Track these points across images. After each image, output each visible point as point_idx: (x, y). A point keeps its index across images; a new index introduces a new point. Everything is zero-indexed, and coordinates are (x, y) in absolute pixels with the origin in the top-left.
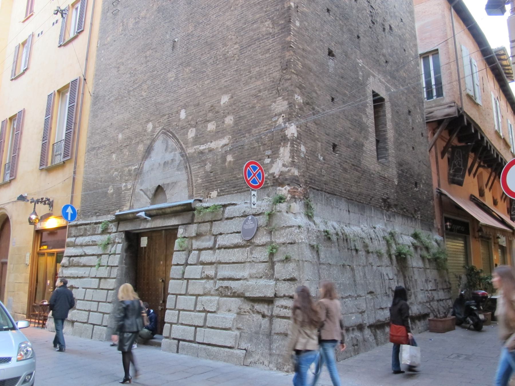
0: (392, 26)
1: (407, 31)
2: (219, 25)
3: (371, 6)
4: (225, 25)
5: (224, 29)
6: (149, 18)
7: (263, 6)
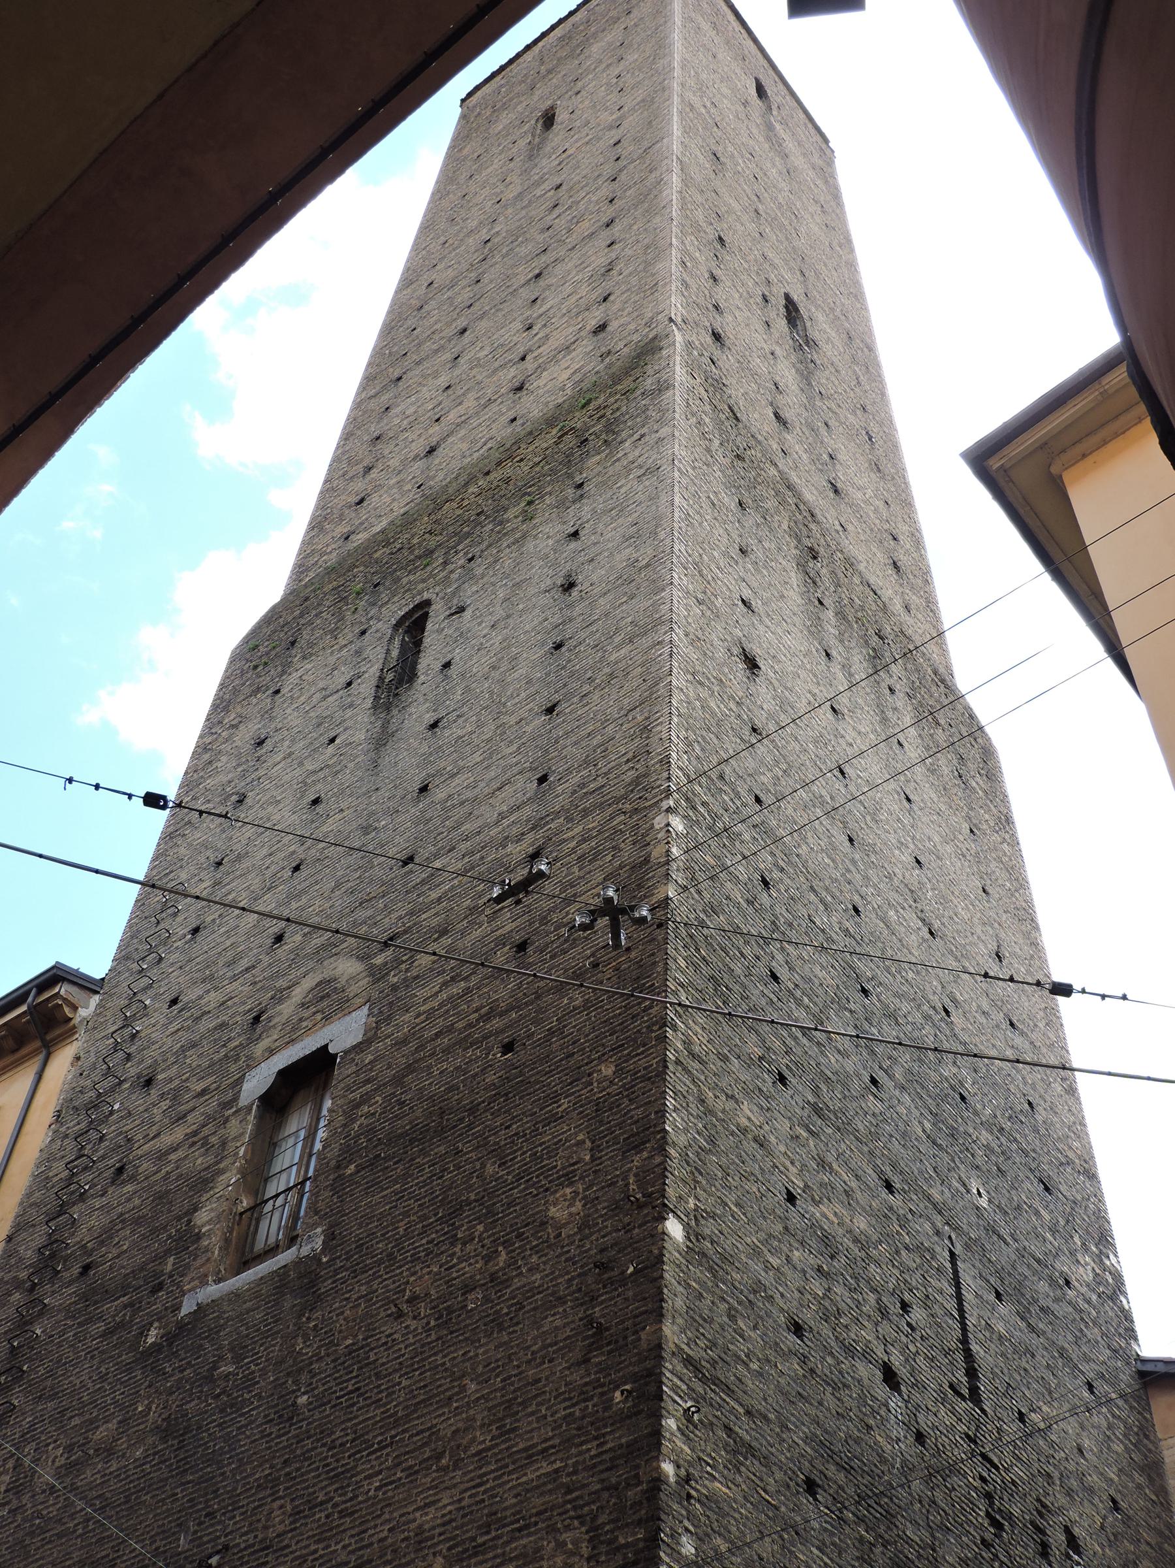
0: (1076, 1531)
1: (1144, 1547)
2: (389, 1521)
3: (984, 1456)
4: (413, 1526)
6: (123, 1456)
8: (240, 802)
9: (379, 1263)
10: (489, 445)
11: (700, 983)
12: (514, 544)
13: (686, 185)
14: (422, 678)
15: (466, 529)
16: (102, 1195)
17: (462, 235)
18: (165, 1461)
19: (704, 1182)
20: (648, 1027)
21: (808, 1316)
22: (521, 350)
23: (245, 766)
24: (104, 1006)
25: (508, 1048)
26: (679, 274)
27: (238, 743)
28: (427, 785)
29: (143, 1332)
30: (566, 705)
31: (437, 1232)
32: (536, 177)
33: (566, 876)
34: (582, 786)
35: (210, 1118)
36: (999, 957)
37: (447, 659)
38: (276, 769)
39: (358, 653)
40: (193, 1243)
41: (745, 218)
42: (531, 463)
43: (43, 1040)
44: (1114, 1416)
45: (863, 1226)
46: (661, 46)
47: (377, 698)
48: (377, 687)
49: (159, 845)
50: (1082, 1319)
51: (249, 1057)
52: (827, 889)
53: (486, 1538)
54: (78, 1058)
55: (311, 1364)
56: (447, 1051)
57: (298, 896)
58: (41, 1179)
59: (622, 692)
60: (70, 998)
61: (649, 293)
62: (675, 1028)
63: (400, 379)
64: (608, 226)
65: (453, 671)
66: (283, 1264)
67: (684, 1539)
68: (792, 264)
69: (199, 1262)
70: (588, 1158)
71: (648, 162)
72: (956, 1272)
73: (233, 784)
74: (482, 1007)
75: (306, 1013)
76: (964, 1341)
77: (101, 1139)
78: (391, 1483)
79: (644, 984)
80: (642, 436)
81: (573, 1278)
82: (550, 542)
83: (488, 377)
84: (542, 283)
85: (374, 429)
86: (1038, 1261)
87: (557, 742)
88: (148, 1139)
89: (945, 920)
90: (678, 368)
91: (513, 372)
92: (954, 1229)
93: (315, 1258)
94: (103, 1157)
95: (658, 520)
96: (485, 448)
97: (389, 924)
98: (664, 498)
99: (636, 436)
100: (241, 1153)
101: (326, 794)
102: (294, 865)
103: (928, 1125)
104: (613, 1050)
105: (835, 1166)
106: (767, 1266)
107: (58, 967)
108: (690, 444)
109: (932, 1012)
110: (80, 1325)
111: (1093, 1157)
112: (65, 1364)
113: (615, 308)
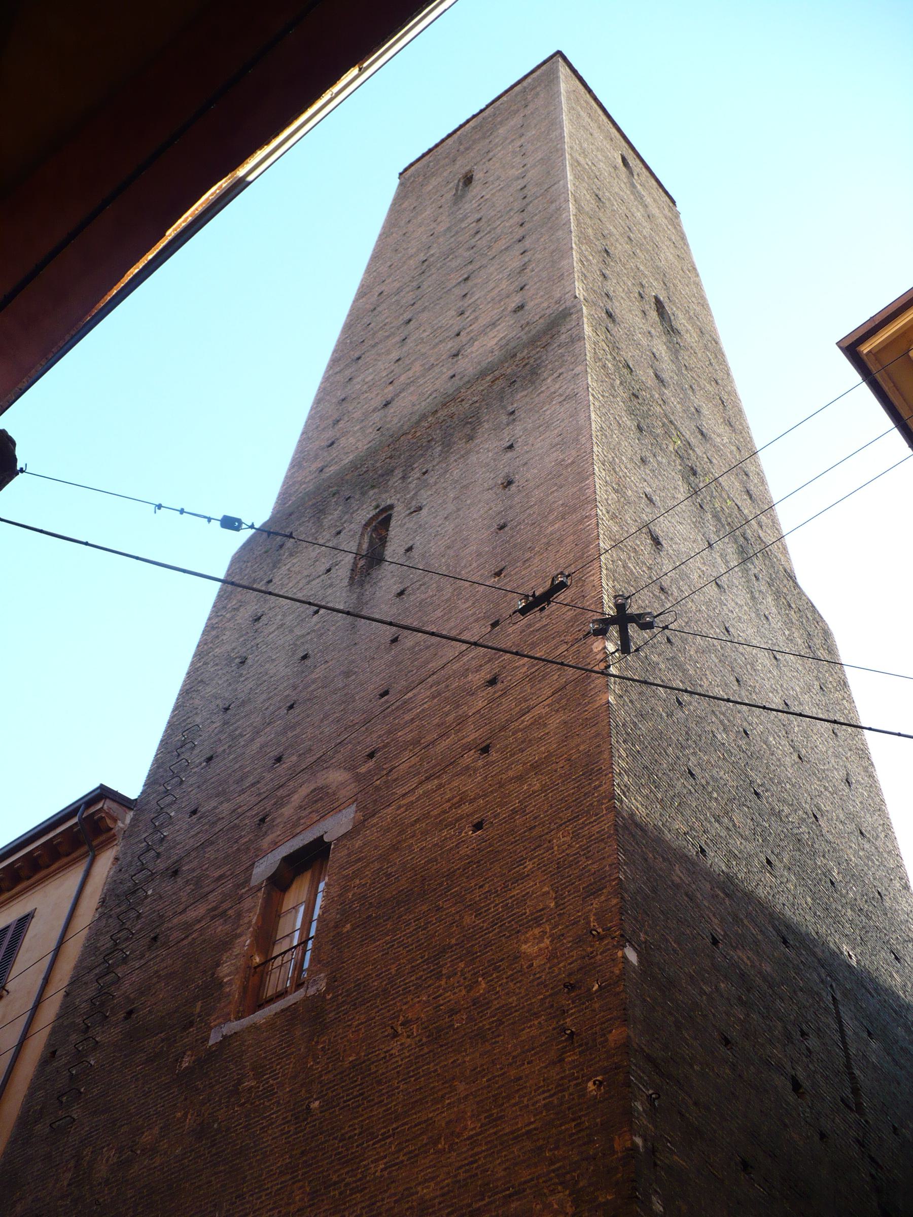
2: (395, 1194)
3: (873, 1159)
5: (410, 1208)
6: (166, 1153)
7: (541, 1142)
8: (243, 663)
10: (434, 396)
12: (459, 458)
13: (579, 211)
15: (420, 452)
16: (141, 958)
18: (201, 1156)
20: (598, 801)
22: (456, 329)
23: (245, 637)
24: (137, 820)
25: (478, 826)
26: (579, 268)
28: (397, 637)
29: (178, 1059)
30: (512, 568)
31: (424, 970)
32: (461, 216)
33: (520, 693)
36: (848, 782)
38: (270, 636)
41: (621, 240)
42: (470, 402)
43: (90, 846)
45: (769, 969)
46: (555, 123)
48: (352, 570)
49: (178, 699)
51: (258, 849)
53: (481, 1203)
54: (116, 859)
55: (321, 1076)
57: (293, 728)
58: (90, 947)
59: (559, 555)
61: (556, 281)
63: (359, 358)
64: (520, 241)
67: (654, 1199)
68: (657, 276)
70: (552, 905)
71: (549, 197)
72: (838, 1013)
73: (236, 651)
74: (453, 797)
75: (304, 814)
76: (848, 1066)
77: (139, 916)
79: (593, 769)
80: (560, 374)
81: (546, 998)
82: (490, 454)
83: (430, 349)
84: (470, 283)
85: (340, 394)
86: (895, 1011)
88: (175, 914)
90: (586, 326)
92: (834, 980)
93: (320, 996)
94: (141, 930)
95: (579, 430)
96: (431, 397)
98: (582, 416)
99: (556, 375)
100: (254, 921)
102: (289, 704)
104: (569, 821)
105: (746, 922)
106: (702, 992)
107: (102, 787)
109: (805, 816)
112: (115, 1086)
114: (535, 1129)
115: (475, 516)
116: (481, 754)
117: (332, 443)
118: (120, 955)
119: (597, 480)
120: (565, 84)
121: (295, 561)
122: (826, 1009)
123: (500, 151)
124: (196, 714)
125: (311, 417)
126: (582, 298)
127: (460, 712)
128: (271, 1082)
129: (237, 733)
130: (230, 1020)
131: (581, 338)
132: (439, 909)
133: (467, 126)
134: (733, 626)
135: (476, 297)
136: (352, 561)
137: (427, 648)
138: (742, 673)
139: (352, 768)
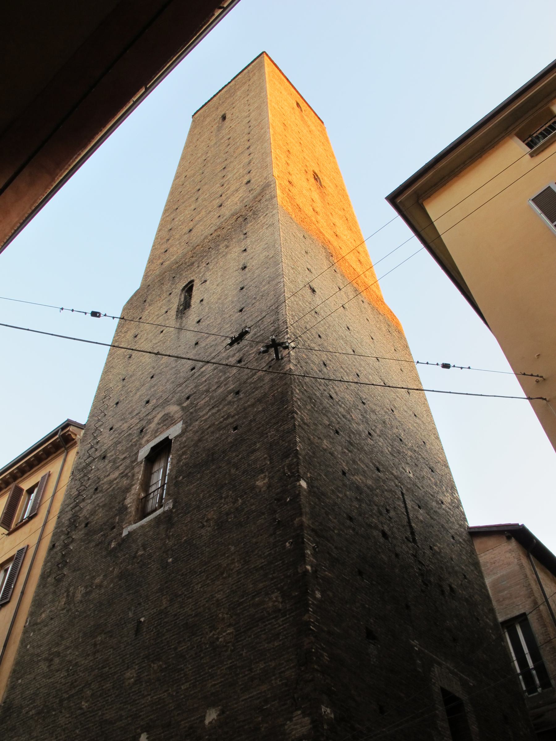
0: (453, 586)
2: (205, 598)
4: (215, 599)
6: (106, 587)
8: (130, 357)
9: (194, 509)
11: (305, 399)
14: (193, 306)
15: (205, 254)
16: (91, 499)
17: (196, 159)
19: (312, 468)
21: (354, 514)
22: (220, 193)
25: (235, 429)
27: (128, 338)
28: (198, 342)
29: (109, 544)
32: (221, 137)
34: (255, 334)
35: (127, 467)
37: (202, 299)
39: (169, 301)
40: (125, 511)
43: (65, 448)
44: (462, 547)
45: (370, 483)
47: (177, 315)
48: (177, 311)
49: (102, 376)
50: (448, 515)
52: (347, 368)
54: (78, 453)
56: (213, 433)
57: (154, 387)
58: (68, 495)
60: (74, 432)
62: (297, 414)
64: (248, 149)
65: (204, 302)
66: (158, 514)
67: (317, 592)
69: (128, 517)
70: (269, 463)
71: (261, 126)
72: (404, 499)
75: (160, 426)
76: (409, 522)
77: (89, 479)
78: (205, 585)
80: (267, 214)
81: (267, 505)
84: (226, 170)
86: (432, 495)
87: (244, 321)
88: (105, 477)
89: (389, 380)
90: (278, 190)
91: (218, 201)
93: (170, 511)
95: (275, 241)
97: (188, 391)
98: (276, 234)
99: (265, 215)
100: (140, 478)
101: (161, 350)
102: (151, 376)
103: (390, 449)
105: (359, 462)
107: (68, 420)
108: (284, 216)
109: (387, 411)
110: (86, 544)
111: (447, 460)
113: (253, 175)
114: (265, 565)
115: (230, 284)
116: (236, 395)
117: (166, 251)
118: (81, 498)
119: (283, 264)
120: (268, 68)
121: (151, 308)
122: (398, 498)
123: (238, 103)
124: (110, 382)
125: (156, 238)
126: (277, 176)
127: (226, 376)
128: (151, 551)
129: (129, 390)
130: (131, 524)
131: (275, 196)
132: (220, 467)
133: (223, 91)
134: (351, 326)
135: (229, 177)
136: (177, 307)
137: (211, 346)
138: (356, 348)
139: (180, 404)
